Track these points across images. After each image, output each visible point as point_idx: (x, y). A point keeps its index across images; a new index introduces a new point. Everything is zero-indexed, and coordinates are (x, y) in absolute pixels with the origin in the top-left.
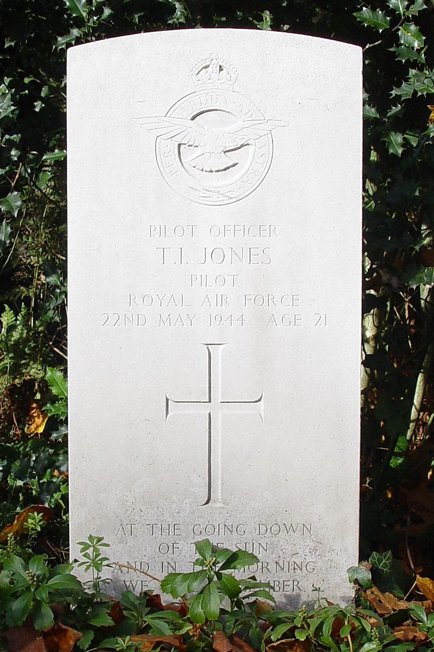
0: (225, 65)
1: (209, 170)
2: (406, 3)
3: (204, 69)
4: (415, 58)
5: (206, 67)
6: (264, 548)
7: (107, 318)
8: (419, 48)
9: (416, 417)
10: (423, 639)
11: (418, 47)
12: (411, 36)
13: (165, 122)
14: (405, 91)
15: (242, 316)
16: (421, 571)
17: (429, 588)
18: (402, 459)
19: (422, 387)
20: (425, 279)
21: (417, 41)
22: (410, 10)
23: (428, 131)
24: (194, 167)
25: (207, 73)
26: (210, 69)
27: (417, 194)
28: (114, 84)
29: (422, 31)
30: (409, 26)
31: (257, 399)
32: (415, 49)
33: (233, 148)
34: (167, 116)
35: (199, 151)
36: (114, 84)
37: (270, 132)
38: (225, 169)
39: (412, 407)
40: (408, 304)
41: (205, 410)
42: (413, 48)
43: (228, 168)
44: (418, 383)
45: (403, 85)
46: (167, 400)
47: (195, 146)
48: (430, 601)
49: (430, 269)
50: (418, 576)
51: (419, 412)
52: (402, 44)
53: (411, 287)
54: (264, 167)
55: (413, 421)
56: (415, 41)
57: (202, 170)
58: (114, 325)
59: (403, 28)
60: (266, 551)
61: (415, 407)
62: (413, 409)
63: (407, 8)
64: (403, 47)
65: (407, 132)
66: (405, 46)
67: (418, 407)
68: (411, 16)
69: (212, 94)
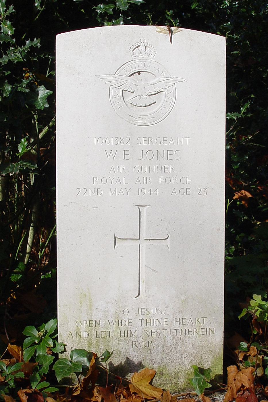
0: (149, 46)
1: (140, 106)
2: (5, 8)
3: (137, 48)
4: (9, 41)
5: (137, 47)
6: (98, 324)
7: (79, 191)
8: (11, 35)
9: (30, 250)
10: (3, 381)
11: (11, 34)
12: (7, 28)
13: (114, 78)
14: (4, 60)
15: (157, 189)
16: (15, 341)
17: (16, 351)
18: (21, 276)
19: (32, 233)
20: (10, 170)
21: (10, 31)
22: (7, 12)
23: (22, 84)
24: (131, 104)
25: (151, 52)
26: (140, 48)
27: (5, 120)
28: (86, 59)
29: (13, 25)
30: (6, 22)
31: (166, 238)
32: (9, 35)
33: (154, 93)
34: (116, 74)
35: (134, 95)
36: (86, 59)
37: (174, 84)
38: (148, 106)
39: (27, 245)
40: (24, 185)
41: (137, 243)
42: (8, 35)
43: (151, 105)
44: (30, 231)
45: (3, 57)
46: (115, 237)
47: (132, 92)
48: (15, 359)
49: (13, 164)
50: (9, 344)
51: (31, 248)
52: (2, 33)
53: (2, 175)
54: (171, 104)
55: (28, 253)
56: (9, 31)
57: (136, 106)
58: (84, 195)
59: (3, 23)
60: (99, 325)
61: (29, 245)
62: (28, 246)
63: (6, 11)
64: (2, 34)
65: (15, 84)
66: (4, 33)
67: (30, 245)
68: (6, 16)
69: (145, 62)
